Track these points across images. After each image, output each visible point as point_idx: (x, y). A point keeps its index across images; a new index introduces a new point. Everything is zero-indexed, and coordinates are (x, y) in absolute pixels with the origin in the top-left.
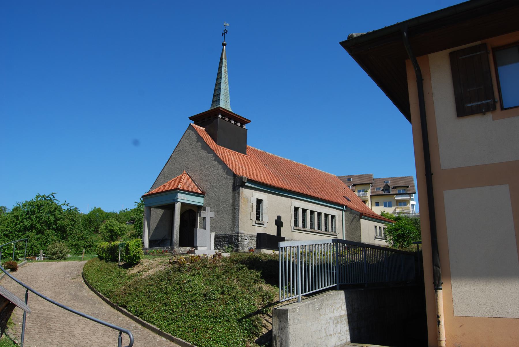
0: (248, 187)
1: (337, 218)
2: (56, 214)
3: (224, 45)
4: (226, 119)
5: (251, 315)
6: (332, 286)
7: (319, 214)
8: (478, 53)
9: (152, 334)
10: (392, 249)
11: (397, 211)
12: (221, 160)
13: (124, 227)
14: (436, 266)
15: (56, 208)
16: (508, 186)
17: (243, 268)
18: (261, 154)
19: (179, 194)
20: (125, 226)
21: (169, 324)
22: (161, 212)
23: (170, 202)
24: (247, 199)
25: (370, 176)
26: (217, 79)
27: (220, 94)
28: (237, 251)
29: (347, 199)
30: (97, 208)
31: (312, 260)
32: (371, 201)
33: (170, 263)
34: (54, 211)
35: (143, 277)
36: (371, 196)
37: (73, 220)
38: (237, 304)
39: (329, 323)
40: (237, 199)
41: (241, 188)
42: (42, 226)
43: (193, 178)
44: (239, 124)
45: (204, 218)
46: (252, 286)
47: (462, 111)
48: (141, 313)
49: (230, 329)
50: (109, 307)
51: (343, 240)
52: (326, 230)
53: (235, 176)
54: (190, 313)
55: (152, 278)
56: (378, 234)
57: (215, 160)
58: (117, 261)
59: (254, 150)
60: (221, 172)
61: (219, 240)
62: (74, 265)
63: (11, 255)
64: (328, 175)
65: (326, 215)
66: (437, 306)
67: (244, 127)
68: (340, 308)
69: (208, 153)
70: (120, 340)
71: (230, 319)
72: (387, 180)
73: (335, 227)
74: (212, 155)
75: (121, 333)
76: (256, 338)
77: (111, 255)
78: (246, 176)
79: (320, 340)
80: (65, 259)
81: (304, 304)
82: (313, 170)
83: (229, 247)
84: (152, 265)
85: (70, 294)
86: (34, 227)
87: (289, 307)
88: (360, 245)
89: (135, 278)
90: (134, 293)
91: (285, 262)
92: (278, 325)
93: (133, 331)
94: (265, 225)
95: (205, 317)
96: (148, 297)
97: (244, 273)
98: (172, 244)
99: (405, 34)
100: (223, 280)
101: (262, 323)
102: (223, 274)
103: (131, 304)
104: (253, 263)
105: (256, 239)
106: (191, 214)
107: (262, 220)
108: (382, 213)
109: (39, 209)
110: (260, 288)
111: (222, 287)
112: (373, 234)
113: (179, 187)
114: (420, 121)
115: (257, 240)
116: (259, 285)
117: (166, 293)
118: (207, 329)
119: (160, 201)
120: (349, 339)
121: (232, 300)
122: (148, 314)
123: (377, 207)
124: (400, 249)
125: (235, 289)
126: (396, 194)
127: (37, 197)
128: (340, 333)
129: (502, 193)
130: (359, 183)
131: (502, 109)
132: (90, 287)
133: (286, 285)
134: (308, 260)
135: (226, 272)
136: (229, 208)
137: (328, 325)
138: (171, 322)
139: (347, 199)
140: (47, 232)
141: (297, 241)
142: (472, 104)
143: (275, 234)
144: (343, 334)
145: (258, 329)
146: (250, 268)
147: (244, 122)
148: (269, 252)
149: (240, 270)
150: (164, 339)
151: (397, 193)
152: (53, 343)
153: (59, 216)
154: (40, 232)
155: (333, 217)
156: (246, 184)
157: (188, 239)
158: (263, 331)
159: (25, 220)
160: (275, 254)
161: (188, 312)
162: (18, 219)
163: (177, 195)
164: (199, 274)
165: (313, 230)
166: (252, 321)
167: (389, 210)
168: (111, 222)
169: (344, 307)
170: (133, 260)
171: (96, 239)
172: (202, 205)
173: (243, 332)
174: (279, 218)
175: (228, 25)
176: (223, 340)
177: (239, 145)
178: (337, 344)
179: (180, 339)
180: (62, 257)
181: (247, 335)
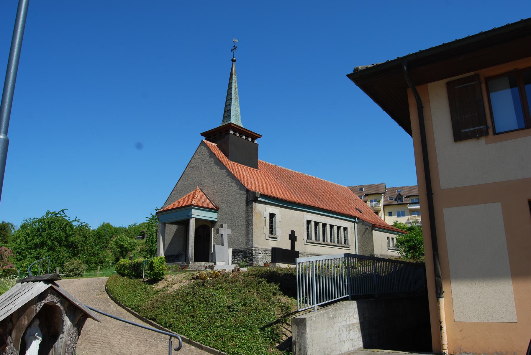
0: (261, 202)
2: (67, 232)
3: (233, 61)
4: (238, 135)
5: (271, 324)
6: (345, 296)
8: (472, 83)
11: (411, 221)
13: (134, 242)
14: (438, 277)
15: (67, 225)
16: (500, 203)
18: (272, 168)
19: (193, 210)
20: (135, 241)
21: (197, 334)
22: (175, 227)
23: (185, 218)
24: (260, 214)
25: (382, 185)
26: (228, 95)
27: (230, 110)
28: (251, 265)
30: (106, 223)
31: (325, 273)
33: (193, 278)
35: (168, 292)
36: (384, 206)
37: (84, 236)
38: (258, 315)
41: (254, 203)
42: (53, 243)
43: (207, 194)
44: (250, 139)
45: (222, 235)
46: (271, 298)
47: (458, 136)
48: (171, 325)
49: (254, 337)
51: (356, 255)
52: (338, 243)
53: (247, 191)
55: (177, 293)
56: (391, 246)
57: (227, 176)
58: (142, 277)
59: (265, 164)
60: (234, 187)
61: (235, 253)
64: (339, 187)
65: (339, 228)
66: (439, 313)
67: (256, 142)
68: (352, 317)
69: (221, 168)
71: (253, 328)
72: (399, 189)
73: (348, 239)
74: (225, 170)
75: (171, 338)
76: (277, 345)
77: (135, 271)
78: (259, 191)
80: (82, 276)
82: (324, 182)
83: (243, 261)
84: (175, 281)
86: (45, 244)
87: (307, 316)
89: (161, 293)
90: (162, 307)
91: (302, 275)
92: (296, 332)
94: (279, 239)
96: (176, 311)
97: (263, 287)
98: (187, 259)
99: (405, 68)
101: (282, 331)
103: (161, 317)
104: (272, 277)
105: (270, 253)
106: (204, 229)
108: (395, 223)
109: (49, 226)
110: (278, 300)
112: (385, 245)
113: (193, 203)
115: (272, 254)
116: (278, 297)
117: (193, 306)
118: (233, 337)
119: (174, 217)
120: (361, 345)
121: (254, 311)
123: (391, 217)
124: (412, 261)
126: (410, 204)
127: (48, 214)
128: (352, 340)
129: (495, 210)
130: (371, 193)
131: (495, 134)
133: (303, 296)
134: (322, 273)
135: (247, 286)
137: (341, 332)
140: (58, 249)
141: (314, 255)
142: (467, 130)
143: (289, 248)
145: (278, 337)
146: (268, 282)
147: (255, 136)
148: (284, 266)
149: (259, 283)
150: (193, 347)
151: (410, 202)
155: (345, 229)
156: (259, 199)
157: (204, 253)
158: (283, 338)
160: (290, 267)
161: (214, 323)
163: (191, 211)
164: (221, 288)
165: (325, 243)
166: (273, 329)
167: (403, 220)
168: (121, 238)
169: (357, 316)
170: (157, 276)
172: (216, 220)
173: (266, 340)
174: (293, 232)
175: (237, 41)
176: (248, 347)
177: (252, 161)
178: (350, 350)
179: (209, 347)
180: (79, 274)
181: (269, 342)
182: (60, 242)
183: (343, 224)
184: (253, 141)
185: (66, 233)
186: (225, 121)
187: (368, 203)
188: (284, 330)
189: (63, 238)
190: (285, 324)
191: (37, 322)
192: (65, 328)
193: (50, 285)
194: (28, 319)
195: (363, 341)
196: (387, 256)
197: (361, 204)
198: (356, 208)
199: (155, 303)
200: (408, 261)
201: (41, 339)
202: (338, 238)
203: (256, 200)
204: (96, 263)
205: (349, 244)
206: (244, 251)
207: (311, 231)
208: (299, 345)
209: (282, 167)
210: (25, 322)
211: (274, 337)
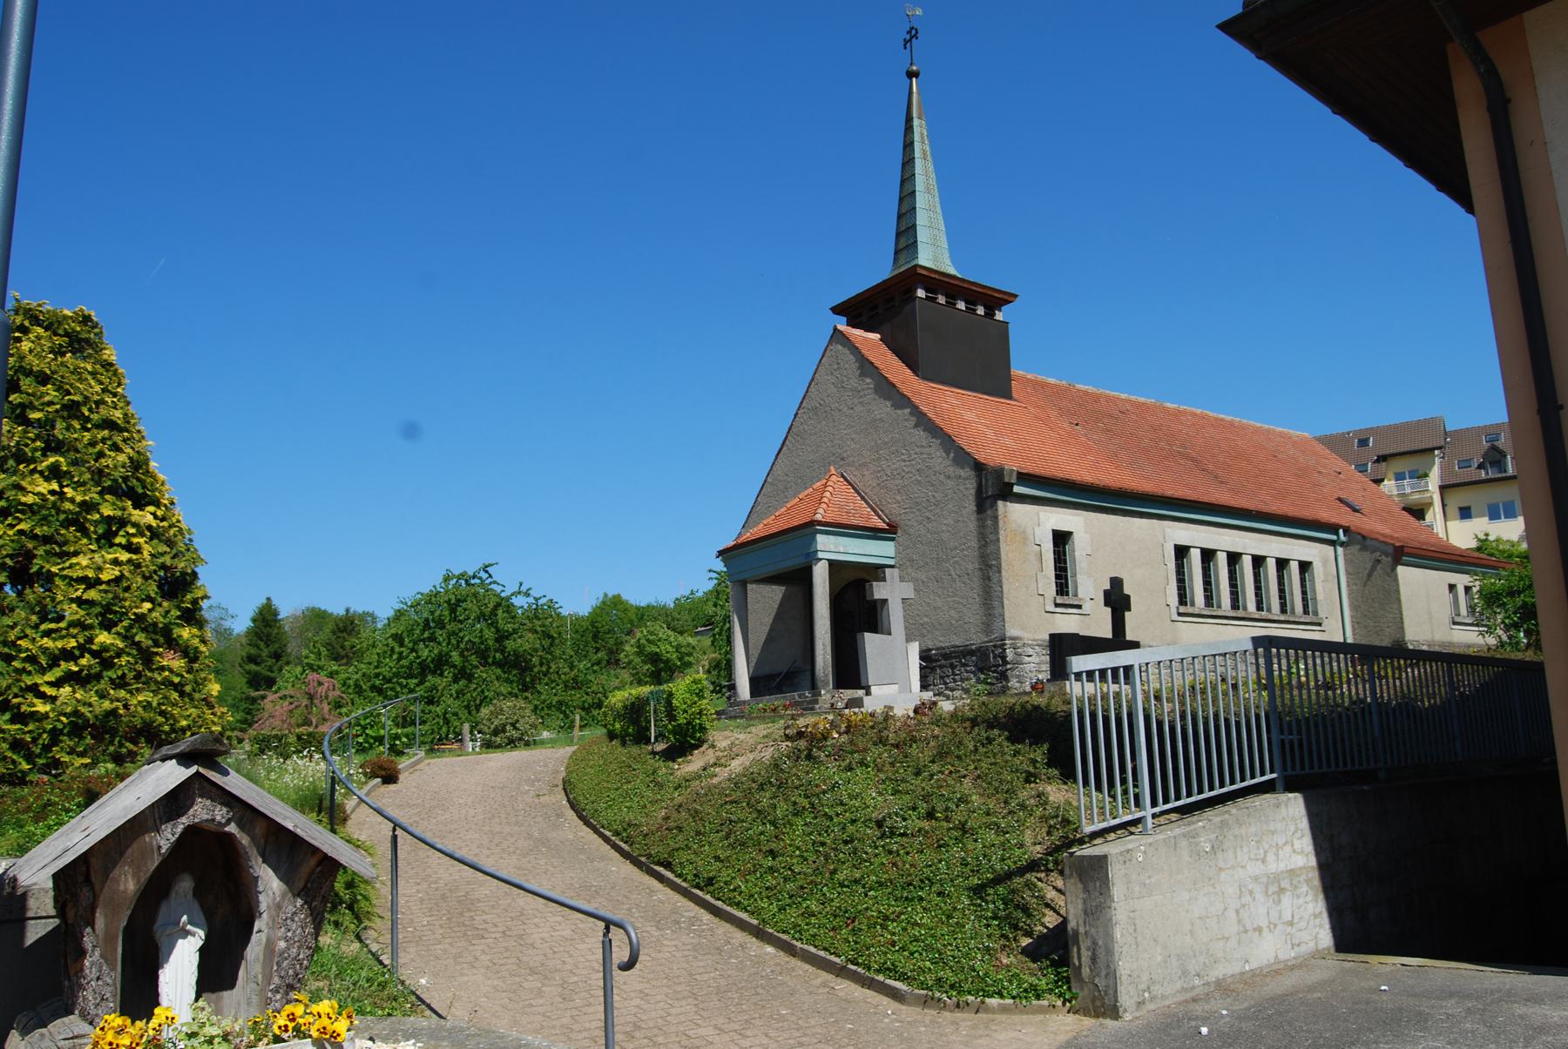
0: (1022, 499)
1: (1318, 568)
3: (911, 75)
4: (942, 299)
5: (1009, 875)
7: (1258, 561)
9: (739, 936)
10: (1493, 659)
12: (933, 423)
15: (498, 605)
17: (990, 741)
18: (1058, 393)
19: (820, 538)
20: (690, 640)
21: (782, 909)
22: (776, 593)
24: (1023, 536)
25: (1433, 424)
26: (903, 182)
27: (914, 226)
29: (1348, 505)
32: (1444, 505)
34: (494, 612)
35: (715, 781)
36: (1443, 488)
39: (1251, 893)
40: (992, 537)
41: (1000, 503)
43: (860, 486)
44: (981, 311)
48: (710, 881)
49: (949, 917)
50: (628, 868)
52: (1283, 611)
53: (979, 467)
54: (840, 876)
57: (916, 426)
58: (648, 741)
60: (939, 459)
61: (934, 666)
62: (549, 758)
63: (380, 740)
64: (1281, 435)
65: (1282, 564)
67: (999, 316)
68: (1288, 848)
69: (896, 406)
70: (607, 946)
71: (948, 889)
73: (1314, 599)
75: (607, 928)
76: (1025, 942)
77: (633, 725)
78: (1013, 465)
79: (1221, 943)
80: (527, 744)
81: (1161, 837)
82: (1232, 424)
83: (979, 681)
84: (739, 747)
85: (530, 836)
88: (1400, 652)
90: (690, 826)
92: (1080, 902)
93: (689, 928)
94: (1087, 608)
95: (880, 884)
98: (814, 687)
100: (932, 776)
101: (1042, 898)
102: (933, 762)
103: (684, 856)
107: (1076, 595)
109: (453, 610)
111: (926, 798)
113: (818, 517)
114: (1507, 237)
117: (773, 823)
118: (886, 918)
119: (769, 560)
120: (1325, 938)
122: (726, 883)
125: (967, 802)
127: (447, 579)
128: (1291, 923)
130: (1398, 452)
132: (581, 817)
135: (942, 754)
136: (970, 566)
137: (1247, 899)
138: (788, 901)
139: (1348, 505)
144: (1303, 924)
145: (1030, 916)
146: (1013, 740)
147: (995, 300)
150: (770, 949)
152: (477, 964)
153: (509, 627)
154: (463, 674)
155: (1305, 566)
156: (1017, 489)
158: (1046, 920)
159: (421, 645)
161: (834, 872)
162: (402, 645)
163: (814, 539)
164: (862, 763)
165: (1240, 613)
166: (1013, 891)
168: (652, 633)
169: (1305, 843)
171: (617, 682)
173: (988, 926)
174: (1116, 583)
175: (919, 12)
177: (989, 373)
178: (1281, 957)
182: (483, 655)
183: (1297, 550)
184: (990, 314)
185: (498, 630)
186: (901, 261)
187: (1389, 485)
188: (1051, 894)
189: (491, 643)
190: (1054, 874)
191: (185, 885)
192: (264, 902)
193: (194, 769)
194: (136, 875)
195: (1333, 928)
196: (1451, 644)
197: (1358, 486)
198: (1340, 499)
199: (675, 815)
200: (1519, 656)
201: (202, 933)
202: (1282, 596)
203: (1006, 494)
204: (583, 709)
205: (1321, 615)
206: (979, 649)
207: (1191, 580)
208: (1089, 943)
209: (1090, 388)
210: (128, 883)
211: (1014, 916)
